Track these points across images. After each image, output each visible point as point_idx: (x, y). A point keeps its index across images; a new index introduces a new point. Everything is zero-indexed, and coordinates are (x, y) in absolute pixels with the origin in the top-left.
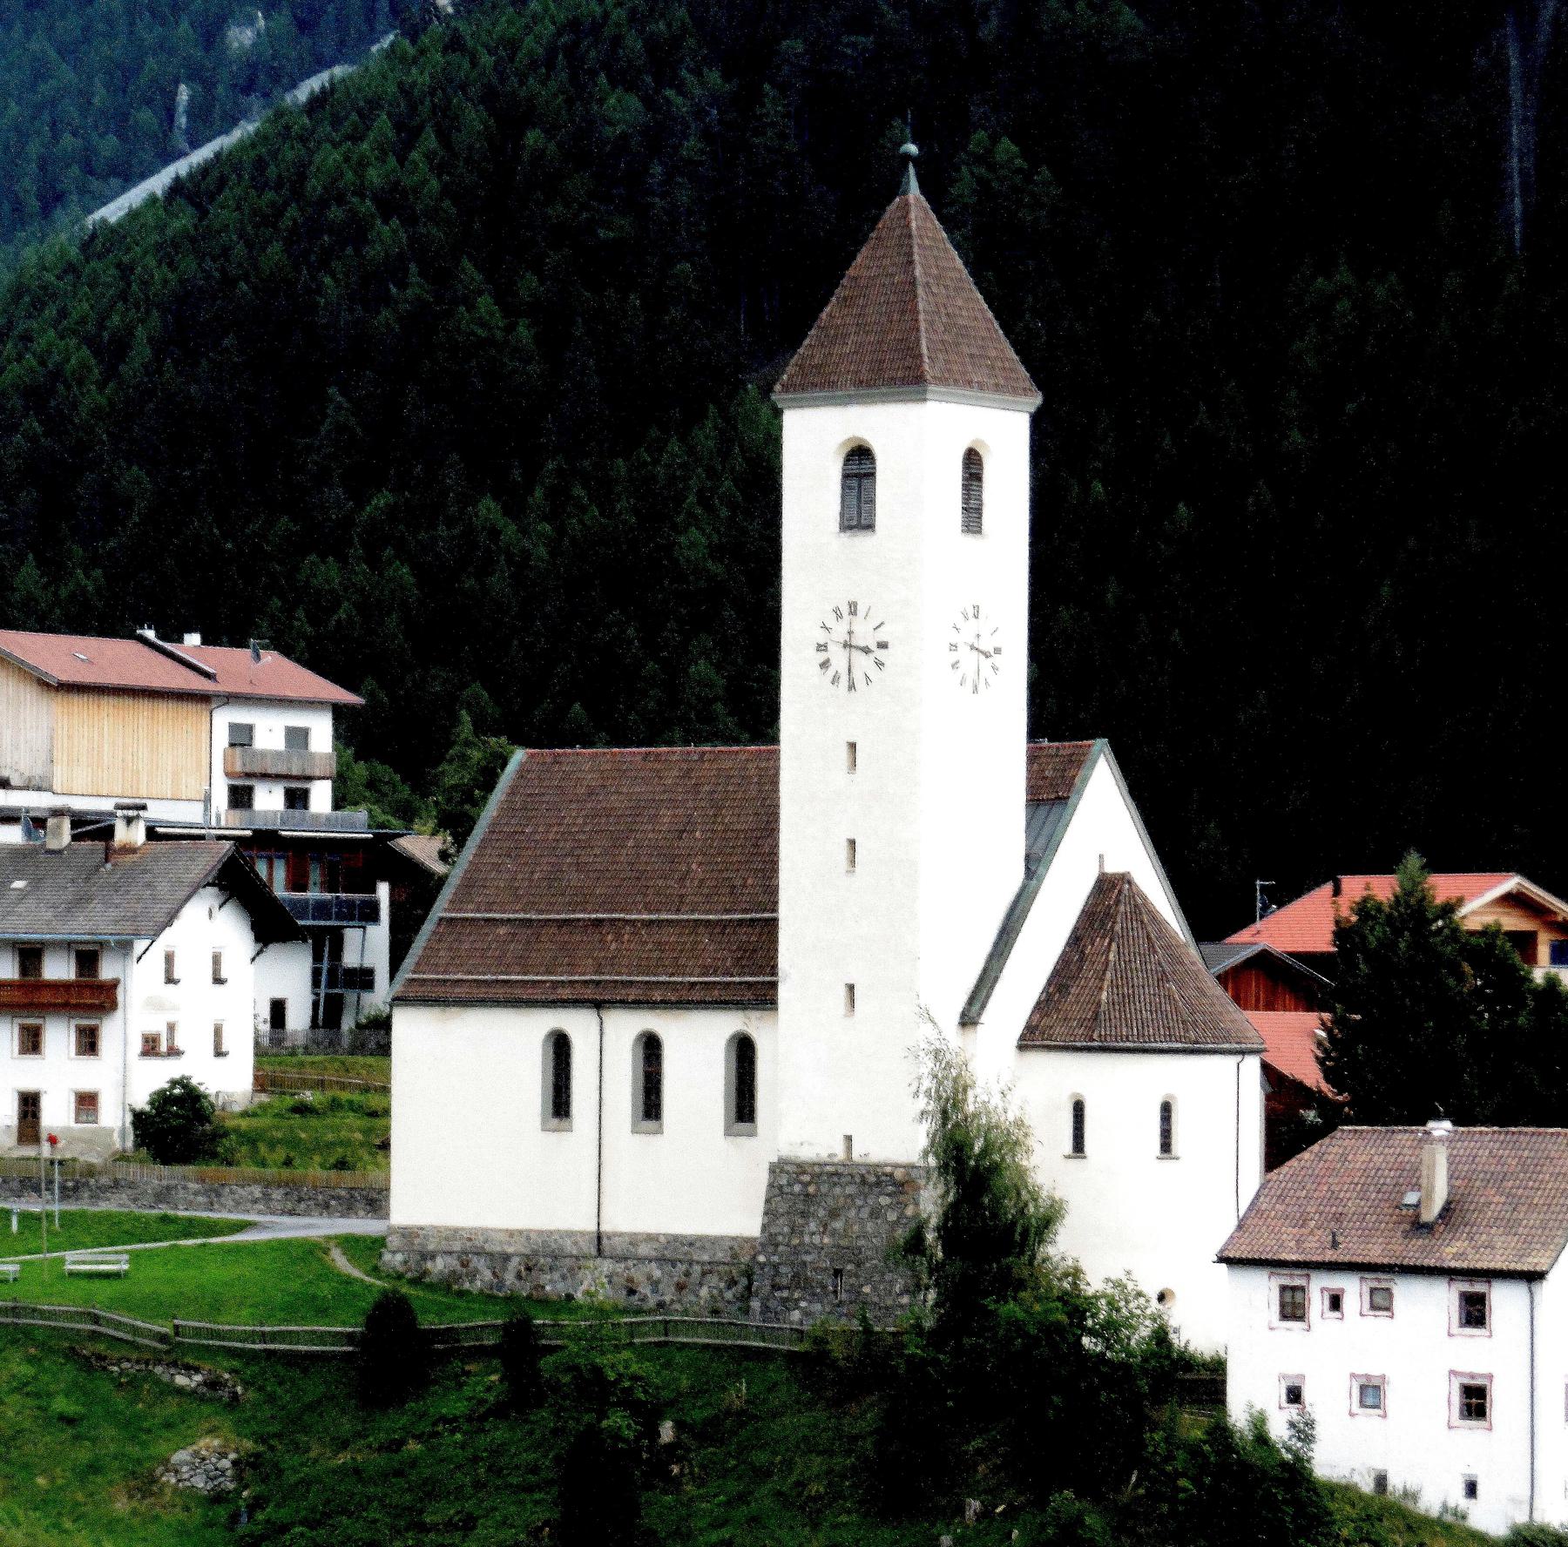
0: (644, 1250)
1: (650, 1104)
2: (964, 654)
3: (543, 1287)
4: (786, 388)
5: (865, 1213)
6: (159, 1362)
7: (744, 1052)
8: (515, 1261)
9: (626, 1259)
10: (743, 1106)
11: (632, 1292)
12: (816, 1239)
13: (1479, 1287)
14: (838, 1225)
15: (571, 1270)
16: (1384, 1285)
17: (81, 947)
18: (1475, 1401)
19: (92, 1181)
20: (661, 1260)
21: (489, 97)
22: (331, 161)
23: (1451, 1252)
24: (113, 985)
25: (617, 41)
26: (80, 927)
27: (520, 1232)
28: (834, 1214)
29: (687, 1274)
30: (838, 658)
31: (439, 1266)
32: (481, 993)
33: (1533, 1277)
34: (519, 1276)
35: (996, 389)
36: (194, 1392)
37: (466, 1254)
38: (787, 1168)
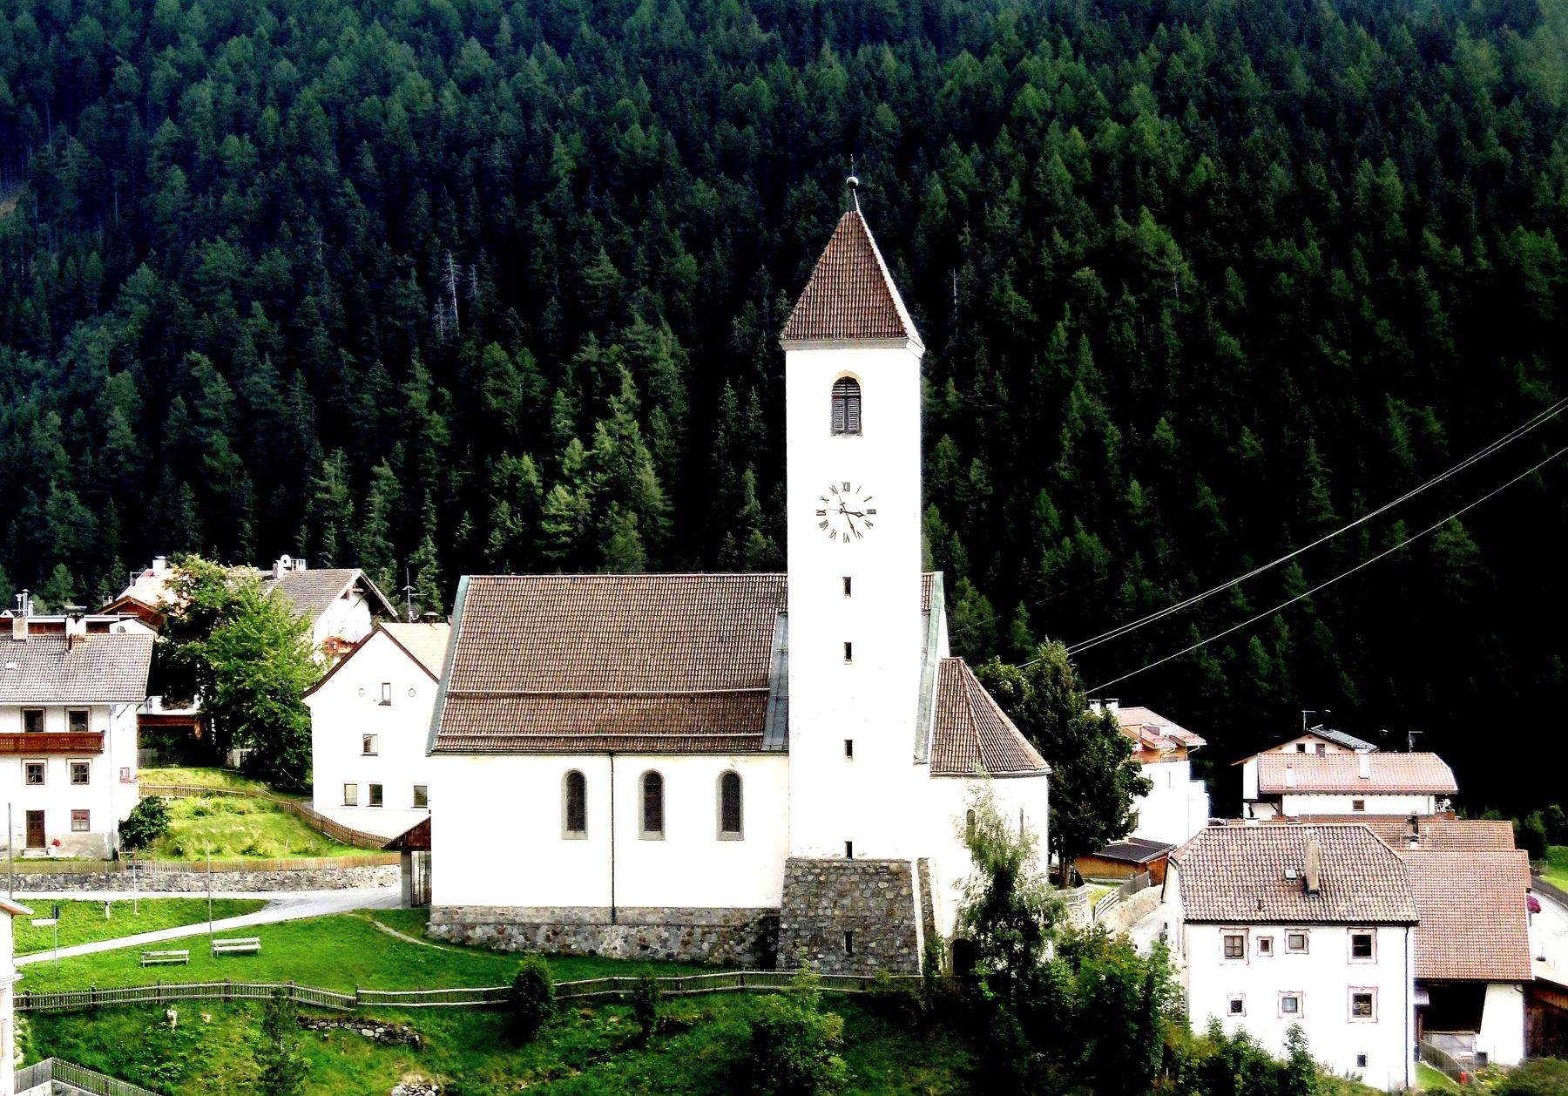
0: (651, 919)
1: (653, 818)
3: (569, 946)
4: (789, 336)
5: (868, 893)
8: (543, 929)
9: (638, 925)
11: (644, 948)
12: (829, 912)
13: (1366, 932)
14: (846, 902)
15: (592, 934)
16: (1300, 933)
17: (73, 709)
18: (1363, 1002)
19: (119, 875)
20: (667, 925)
22: (1057, 167)
23: (1342, 910)
24: (99, 737)
26: (76, 696)
27: (546, 909)
28: (842, 895)
29: (690, 934)
31: (478, 933)
34: (548, 939)
36: (378, 1040)
37: (502, 924)
38: (802, 864)
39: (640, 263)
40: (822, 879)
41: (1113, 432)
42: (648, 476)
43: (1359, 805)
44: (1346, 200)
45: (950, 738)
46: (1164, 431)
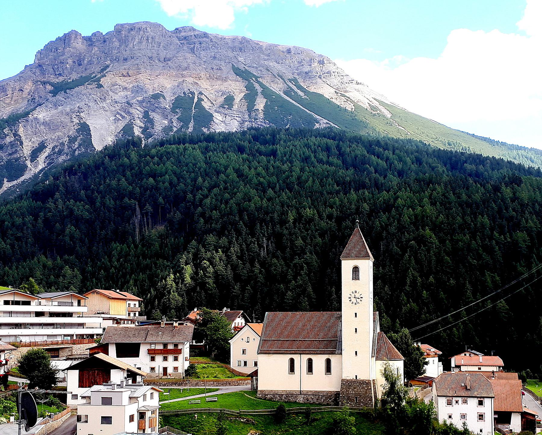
0: (309, 393)
6: (238, 417)
10: (328, 369)
12: (351, 392)
26: (175, 340)
28: (355, 388)
29: (319, 397)
32: (276, 352)
34: (285, 398)
40: (350, 384)
42: (310, 289)
44: (475, 225)
46: (431, 279)
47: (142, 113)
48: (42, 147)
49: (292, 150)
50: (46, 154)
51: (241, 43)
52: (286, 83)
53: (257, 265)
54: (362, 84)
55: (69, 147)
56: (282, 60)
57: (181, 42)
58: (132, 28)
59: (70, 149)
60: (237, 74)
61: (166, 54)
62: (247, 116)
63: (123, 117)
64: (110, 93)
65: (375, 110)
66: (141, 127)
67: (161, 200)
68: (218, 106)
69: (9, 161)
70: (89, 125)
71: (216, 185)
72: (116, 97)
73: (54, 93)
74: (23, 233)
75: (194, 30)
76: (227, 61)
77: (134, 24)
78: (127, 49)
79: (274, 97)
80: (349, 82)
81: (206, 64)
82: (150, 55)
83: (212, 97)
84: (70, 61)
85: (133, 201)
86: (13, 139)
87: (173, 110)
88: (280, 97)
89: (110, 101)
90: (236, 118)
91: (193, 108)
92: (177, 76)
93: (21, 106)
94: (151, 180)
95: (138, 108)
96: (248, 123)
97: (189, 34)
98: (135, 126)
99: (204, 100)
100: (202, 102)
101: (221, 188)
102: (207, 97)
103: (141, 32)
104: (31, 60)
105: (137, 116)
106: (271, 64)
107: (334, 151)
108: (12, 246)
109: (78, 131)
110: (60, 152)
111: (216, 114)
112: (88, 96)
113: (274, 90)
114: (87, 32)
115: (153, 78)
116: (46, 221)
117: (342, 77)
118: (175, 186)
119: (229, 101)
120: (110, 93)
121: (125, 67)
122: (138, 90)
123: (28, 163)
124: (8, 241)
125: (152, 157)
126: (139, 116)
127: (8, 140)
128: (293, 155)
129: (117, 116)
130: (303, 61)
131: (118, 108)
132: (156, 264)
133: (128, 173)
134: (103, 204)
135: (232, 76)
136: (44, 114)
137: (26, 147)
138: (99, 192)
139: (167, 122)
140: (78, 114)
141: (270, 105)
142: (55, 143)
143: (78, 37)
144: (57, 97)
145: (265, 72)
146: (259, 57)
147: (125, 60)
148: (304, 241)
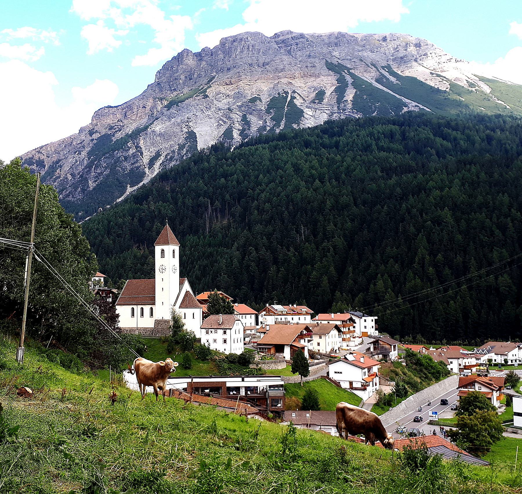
1: (142, 315)
2: (173, 270)
7: (152, 309)
10: (152, 314)
18: (225, 341)
21: (107, 219)
25: (120, 214)
30: (161, 270)
33: (231, 329)
35: (176, 244)
39: (339, 225)
41: (428, 257)
42: (332, 268)
43: (329, 322)
44: (494, 203)
45: (183, 302)
46: (440, 256)
47: (241, 117)
48: (158, 155)
49: (355, 140)
50: (161, 161)
51: (337, 38)
52: (378, 71)
53: (292, 249)
54: (462, 61)
55: (179, 154)
56: (377, 49)
57: (279, 45)
58: (235, 39)
59: (180, 156)
60: (329, 69)
61: (265, 59)
62: (336, 108)
63: (225, 122)
64: (215, 102)
65: (473, 86)
66: (239, 130)
67: (227, 197)
68: (309, 101)
69: (132, 169)
70: (196, 132)
71: (273, 181)
72: (220, 105)
73: (169, 107)
74: (123, 230)
75: (291, 32)
76: (321, 58)
77: (236, 36)
78: (230, 59)
79: (364, 86)
80: (447, 61)
81: (302, 63)
82: (250, 62)
83: (304, 94)
84: (183, 77)
85: (206, 199)
86: (134, 151)
87: (268, 111)
88: (371, 84)
89: (215, 109)
90: (325, 111)
91: (286, 106)
92: (273, 78)
93: (144, 121)
94: (223, 180)
95: (238, 113)
96: (337, 114)
97: (287, 37)
98: (234, 129)
99: (297, 98)
100: (295, 100)
101: (277, 183)
102: (299, 95)
103: (243, 42)
104: (152, 80)
105: (236, 120)
106: (365, 54)
107: (398, 136)
108: (114, 242)
109: (186, 139)
110: (171, 159)
111: (307, 109)
112: (196, 107)
113: (366, 79)
114: (196, 49)
115: (253, 84)
116: (140, 220)
117: (440, 57)
118: (240, 184)
119: (320, 95)
120: (215, 102)
121: (228, 76)
122: (238, 95)
123: (147, 170)
124: (111, 237)
125: (227, 160)
126: (238, 120)
127: (131, 152)
128: (355, 145)
129: (220, 122)
130: (399, 47)
131: (221, 114)
132: (217, 252)
133: (206, 176)
134: (184, 203)
135: (326, 71)
136: (160, 127)
137: (146, 157)
138: (182, 194)
139: (261, 123)
140: (187, 124)
141: (359, 95)
142: (168, 152)
143: (189, 54)
144: (171, 110)
145: (358, 62)
146: (353, 49)
147: (229, 69)
148: (335, 226)
